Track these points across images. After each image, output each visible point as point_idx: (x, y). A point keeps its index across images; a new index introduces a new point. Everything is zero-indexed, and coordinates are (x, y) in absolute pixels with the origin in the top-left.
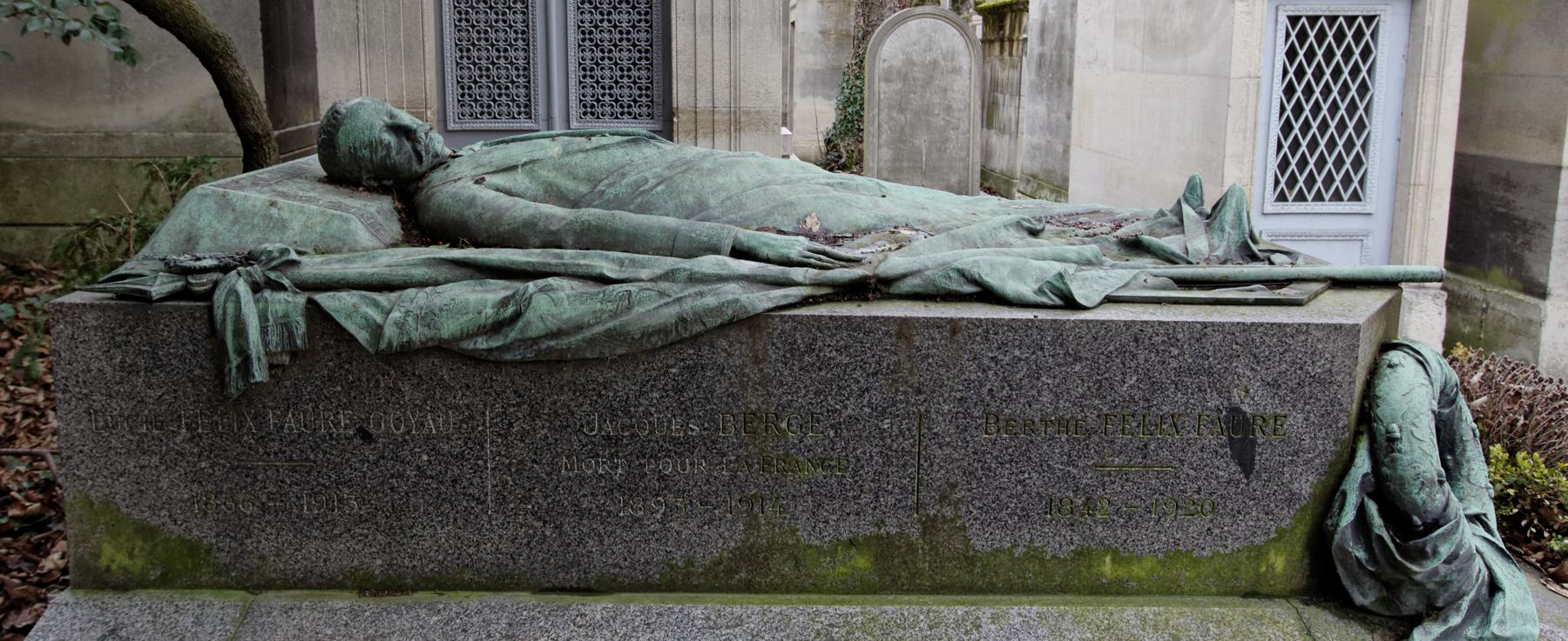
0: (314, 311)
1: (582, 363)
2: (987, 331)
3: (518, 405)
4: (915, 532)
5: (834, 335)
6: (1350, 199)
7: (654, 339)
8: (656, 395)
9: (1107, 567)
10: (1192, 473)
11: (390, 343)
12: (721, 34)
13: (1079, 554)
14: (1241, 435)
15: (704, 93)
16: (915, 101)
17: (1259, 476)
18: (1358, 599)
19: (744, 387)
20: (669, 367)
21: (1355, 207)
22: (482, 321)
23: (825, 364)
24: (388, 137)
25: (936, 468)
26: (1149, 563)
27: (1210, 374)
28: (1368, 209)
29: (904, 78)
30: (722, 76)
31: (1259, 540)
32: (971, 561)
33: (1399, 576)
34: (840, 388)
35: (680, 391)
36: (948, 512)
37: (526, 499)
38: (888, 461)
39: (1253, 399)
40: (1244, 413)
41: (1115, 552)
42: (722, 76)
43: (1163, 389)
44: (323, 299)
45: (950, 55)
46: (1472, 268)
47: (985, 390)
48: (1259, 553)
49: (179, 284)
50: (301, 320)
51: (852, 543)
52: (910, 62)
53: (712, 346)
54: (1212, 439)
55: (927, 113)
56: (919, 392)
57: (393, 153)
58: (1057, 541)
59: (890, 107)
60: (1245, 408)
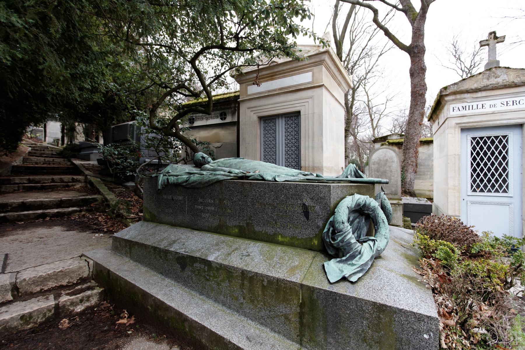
1: (198, 188)
4: (245, 225)
6: (487, 192)
9: (280, 238)
12: (311, 150)
13: (274, 234)
14: (306, 212)
15: (307, 163)
16: (382, 169)
18: (330, 252)
21: (505, 194)
23: (230, 190)
24: (201, 158)
26: (288, 238)
28: (510, 195)
29: (379, 164)
30: (311, 159)
31: (311, 236)
32: (255, 233)
36: (251, 222)
37: (191, 212)
38: (240, 211)
39: (308, 202)
41: (281, 235)
42: (311, 159)
45: (391, 158)
48: (311, 239)
51: (235, 226)
52: (380, 160)
55: (385, 172)
58: (270, 230)
59: (375, 171)
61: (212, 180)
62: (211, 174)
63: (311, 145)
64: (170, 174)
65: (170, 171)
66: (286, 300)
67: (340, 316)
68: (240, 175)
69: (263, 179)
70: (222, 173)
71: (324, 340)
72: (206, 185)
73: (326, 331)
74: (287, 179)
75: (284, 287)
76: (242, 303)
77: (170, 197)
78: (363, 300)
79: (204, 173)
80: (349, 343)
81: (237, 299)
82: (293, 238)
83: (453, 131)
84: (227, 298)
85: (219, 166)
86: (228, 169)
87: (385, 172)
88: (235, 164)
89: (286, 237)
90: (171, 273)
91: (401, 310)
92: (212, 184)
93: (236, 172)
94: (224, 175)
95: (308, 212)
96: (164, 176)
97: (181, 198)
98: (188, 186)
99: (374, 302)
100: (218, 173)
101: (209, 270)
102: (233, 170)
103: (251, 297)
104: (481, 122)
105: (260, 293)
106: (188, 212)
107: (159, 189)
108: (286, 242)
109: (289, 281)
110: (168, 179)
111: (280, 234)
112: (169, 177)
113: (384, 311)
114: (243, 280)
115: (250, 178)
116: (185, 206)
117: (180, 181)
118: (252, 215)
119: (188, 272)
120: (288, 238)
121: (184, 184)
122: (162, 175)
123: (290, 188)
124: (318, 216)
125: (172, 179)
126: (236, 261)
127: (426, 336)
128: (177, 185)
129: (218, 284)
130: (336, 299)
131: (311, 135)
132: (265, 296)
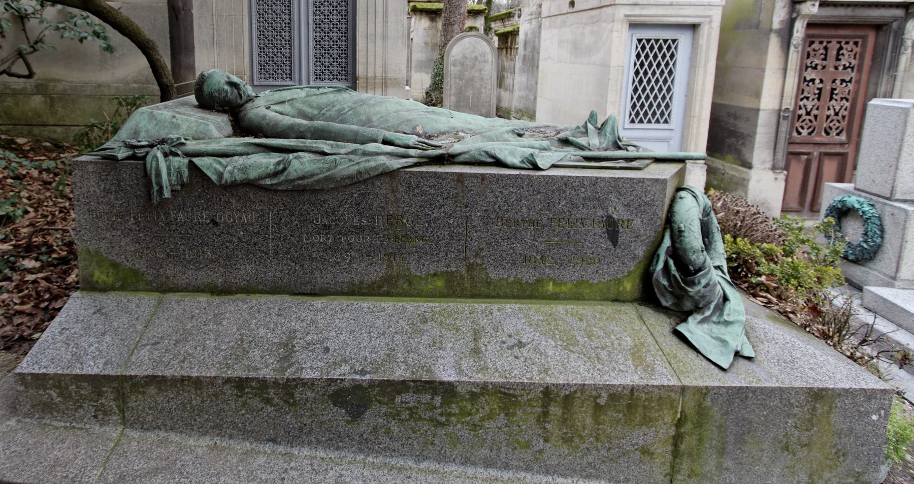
0: (192, 166)
3: (284, 210)
4: (463, 270)
11: (226, 181)
12: (379, 43)
13: (538, 281)
15: (371, 70)
16: (467, 75)
18: (664, 303)
19: (387, 203)
21: (666, 126)
22: (269, 171)
23: (423, 193)
24: (227, 88)
26: (569, 286)
27: (599, 201)
28: (672, 127)
29: (462, 64)
30: (379, 62)
31: (620, 276)
32: (489, 284)
35: (358, 204)
36: (479, 261)
37: (287, 253)
39: (619, 213)
43: (577, 207)
44: (196, 160)
45: (483, 54)
47: (496, 206)
48: (619, 282)
50: (186, 170)
54: (599, 230)
56: (467, 207)
58: (528, 275)
59: (455, 78)
60: (614, 216)
61: (367, 171)
63: (379, 30)
66: (647, 421)
67: (750, 422)
69: (498, 163)
71: (717, 467)
73: (722, 452)
75: (647, 399)
76: (541, 452)
78: (793, 388)
80: (760, 459)
81: (527, 445)
82: (580, 283)
83: (620, 27)
84: (499, 449)
87: (472, 79)
89: (565, 283)
90: (310, 433)
91: (846, 391)
95: (618, 232)
99: (809, 389)
101: (446, 402)
103: (566, 433)
104: (655, 16)
105: (589, 421)
106: (276, 253)
108: (565, 293)
109: (657, 386)
111: (551, 279)
113: (823, 397)
114: (545, 406)
115: (461, 158)
118: (484, 246)
119: (372, 418)
120: (569, 286)
123: (582, 185)
124: (637, 237)
126: (504, 367)
127: (874, 417)
129: (475, 427)
130: (747, 397)
131: (380, 9)
132: (600, 424)
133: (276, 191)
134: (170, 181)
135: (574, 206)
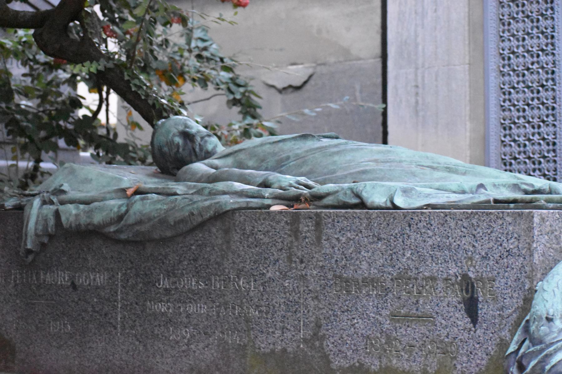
2: (333, 221)
3: (131, 269)
5: (262, 224)
7: (181, 226)
8: (186, 263)
10: (443, 322)
17: (481, 327)
20: (192, 245)
22: (112, 215)
24: (178, 140)
25: (311, 314)
27: (450, 250)
33: (40, 216)
34: (265, 259)
35: (195, 260)
37: (132, 327)
40: (470, 278)
43: (425, 261)
46: (30, 14)
47: (333, 261)
49: (18, 202)
50: (52, 217)
53: (210, 232)
54: (455, 298)
56: (302, 262)
57: (181, 150)
60: (471, 275)
62: (199, 192)
64: (63, 197)
65: (66, 187)
68: (293, 191)
70: (238, 186)
72: (184, 228)
74: (433, 201)
77: (62, 278)
79: (180, 188)
85: (241, 165)
86: (260, 175)
88: (298, 157)
92: (201, 225)
93: (284, 184)
94: (241, 194)
96: (44, 203)
97: (100, 279)
98: (123, 236)
100: (220, 186)
102: (274, 176)
107: (29, 252)
110: (57, 214)
112: (61, 208)
115: (328, 201)
116: (115, 307)
117: (98, 218)
121: (112, 229)
122: (37, 202)
125: (70, 213)
128: (87, 235)
133: (119, 241)
134: (36, 229)
135: (422, 259)
